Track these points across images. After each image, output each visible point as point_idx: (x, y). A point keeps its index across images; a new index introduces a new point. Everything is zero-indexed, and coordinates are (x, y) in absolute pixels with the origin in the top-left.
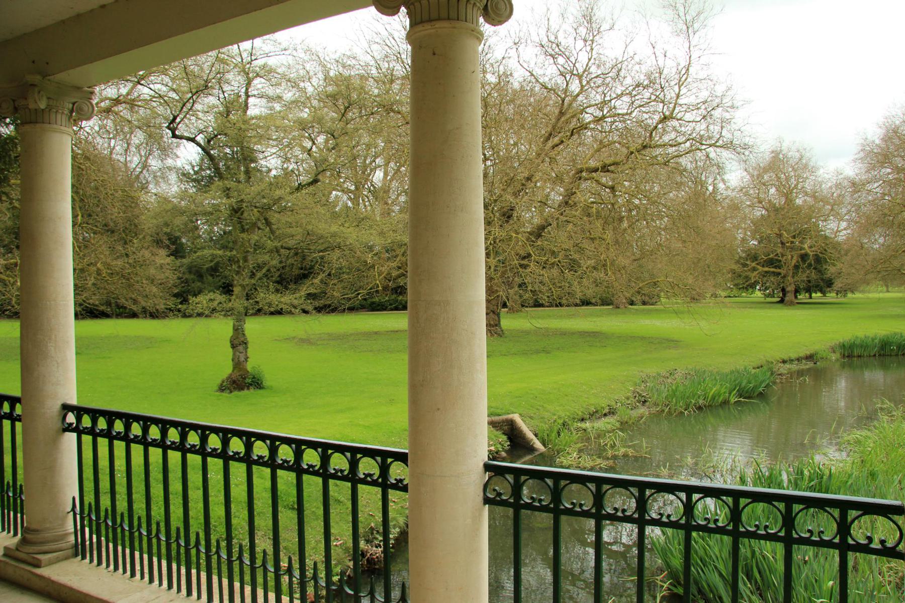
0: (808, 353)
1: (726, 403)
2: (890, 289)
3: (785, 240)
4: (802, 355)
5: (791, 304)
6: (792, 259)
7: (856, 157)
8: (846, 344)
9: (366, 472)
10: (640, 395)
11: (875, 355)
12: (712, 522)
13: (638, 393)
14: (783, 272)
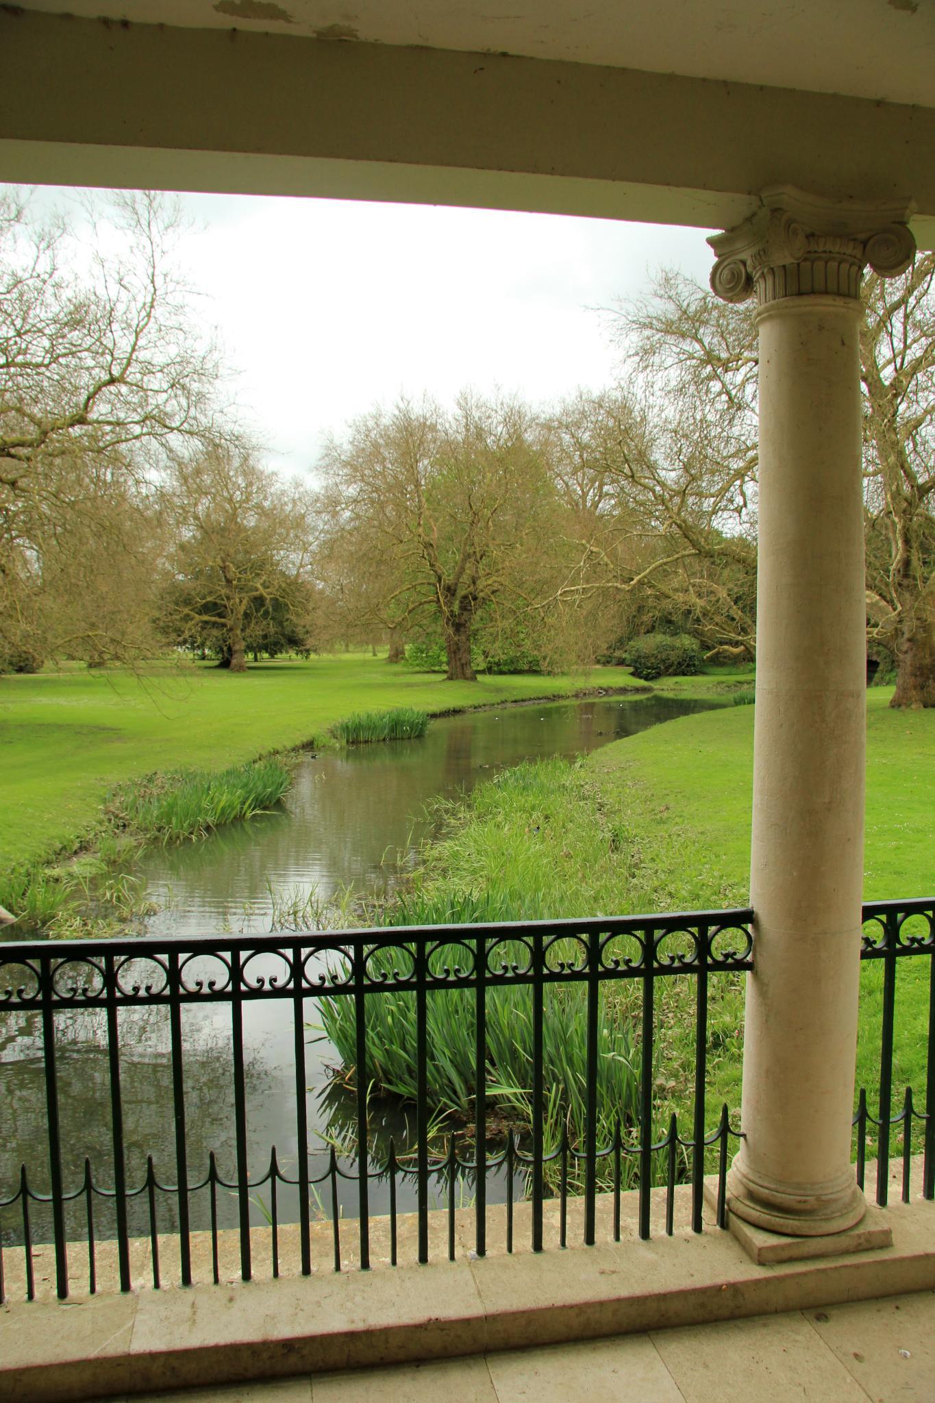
0: (305, 740)
1: (240, 818)
2: (351, 647)
3: (230, 575)
4: (298, 743)
5: (241, 669)
6: (240, 604)
7: (320, 463)
8: (350, 725)
9: (724, 952)
10: (116, 816)
11: (384, 740)
12: (390, 976)
13: (113, 813)
14: (229, 622)
